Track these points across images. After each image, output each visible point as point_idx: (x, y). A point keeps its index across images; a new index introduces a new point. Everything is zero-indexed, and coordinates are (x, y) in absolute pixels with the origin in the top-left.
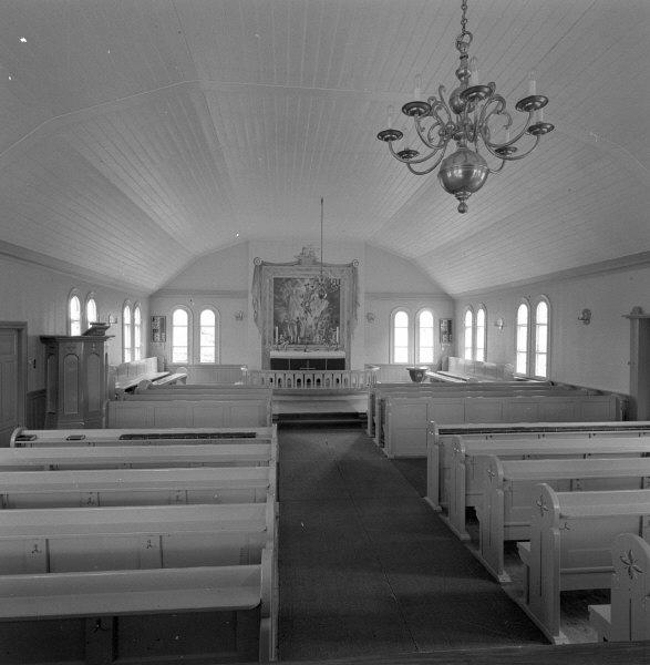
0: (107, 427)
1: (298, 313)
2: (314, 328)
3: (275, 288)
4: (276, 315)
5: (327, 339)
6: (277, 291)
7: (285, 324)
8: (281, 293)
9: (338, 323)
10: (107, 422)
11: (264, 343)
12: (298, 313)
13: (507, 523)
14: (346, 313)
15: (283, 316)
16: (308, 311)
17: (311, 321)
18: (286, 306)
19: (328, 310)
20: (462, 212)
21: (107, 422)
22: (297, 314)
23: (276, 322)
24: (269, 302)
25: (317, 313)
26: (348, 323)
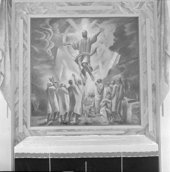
0: (21, 141)
1: (69, 73)
2: (97, 97)
3: (33, 35)
4: (35, 78)
5: (118, 118)
6: (35, 40)
7: (49, 92)
8: (43, 44)
9: (136, 87)
10: (20, 139)
11: (15, 125)
12: (69, 73)
13: (90, 115)
14: (149, 71)
15: (46, 80)
16: (86, 70)
17: (91, 86)
18: (52, 63)
19: (119, 68)
20: (94, 96)
21: (20, 139)
22: (69, 75)
23: (35, 89)
24: (24, 60)
25: (101, 74)
26: (154, 88)
